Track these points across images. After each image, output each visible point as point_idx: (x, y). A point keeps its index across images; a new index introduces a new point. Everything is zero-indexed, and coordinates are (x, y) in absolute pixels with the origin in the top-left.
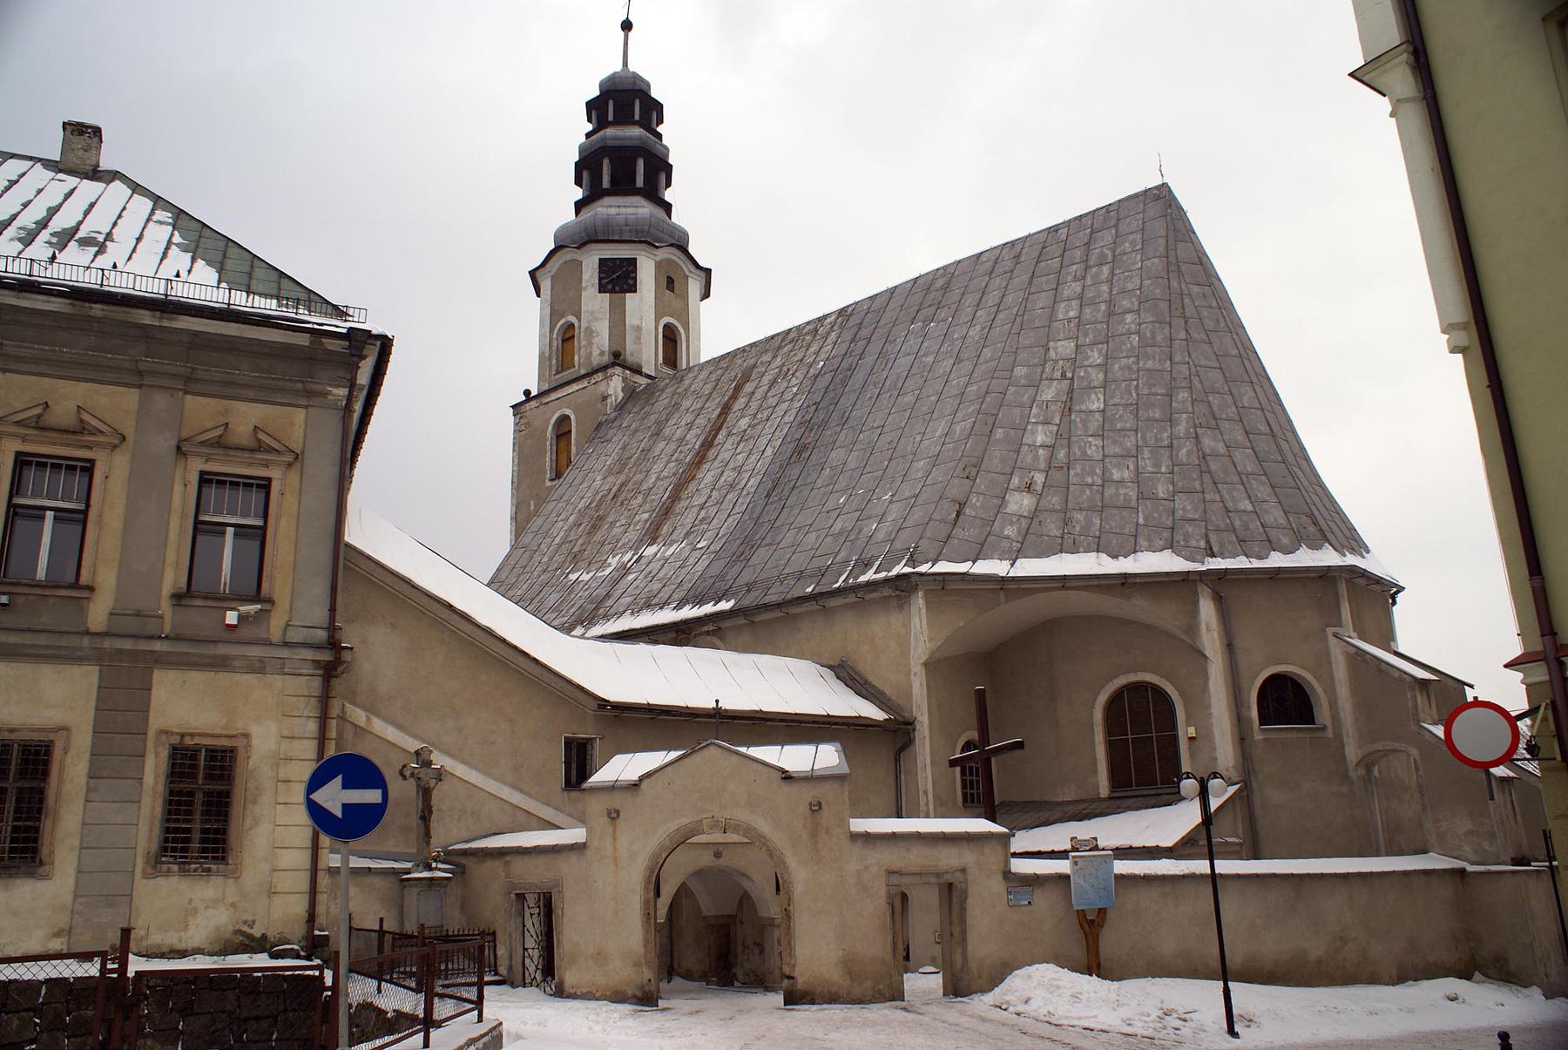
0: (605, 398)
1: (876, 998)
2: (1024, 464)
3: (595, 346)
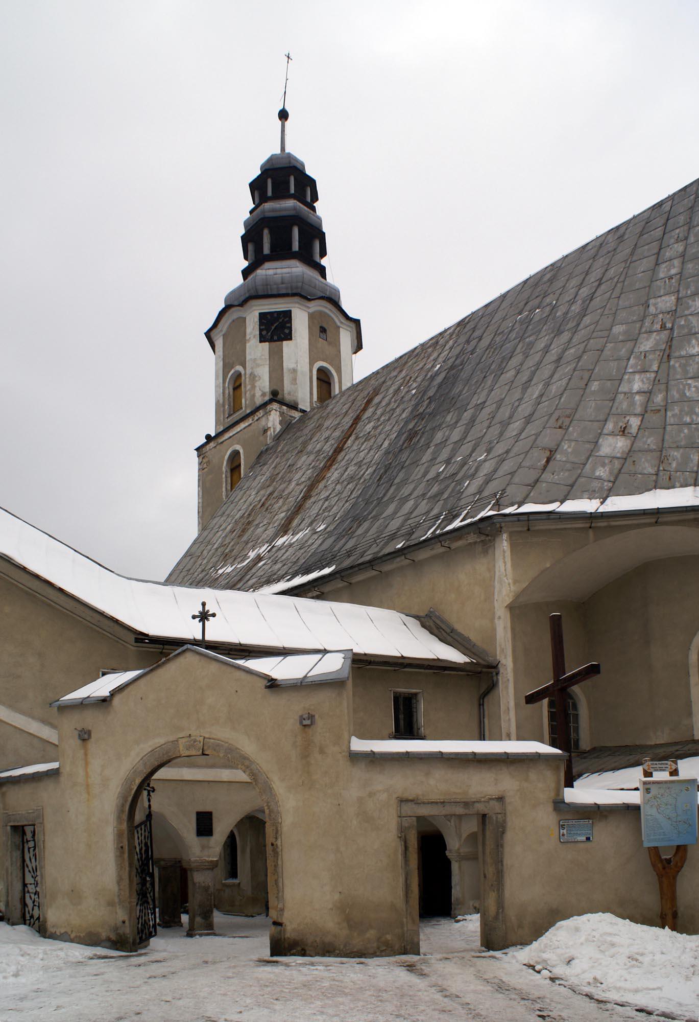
0: (265, 431)
1: (382, 951)
2: (619, 410)
3: (257, 389)
